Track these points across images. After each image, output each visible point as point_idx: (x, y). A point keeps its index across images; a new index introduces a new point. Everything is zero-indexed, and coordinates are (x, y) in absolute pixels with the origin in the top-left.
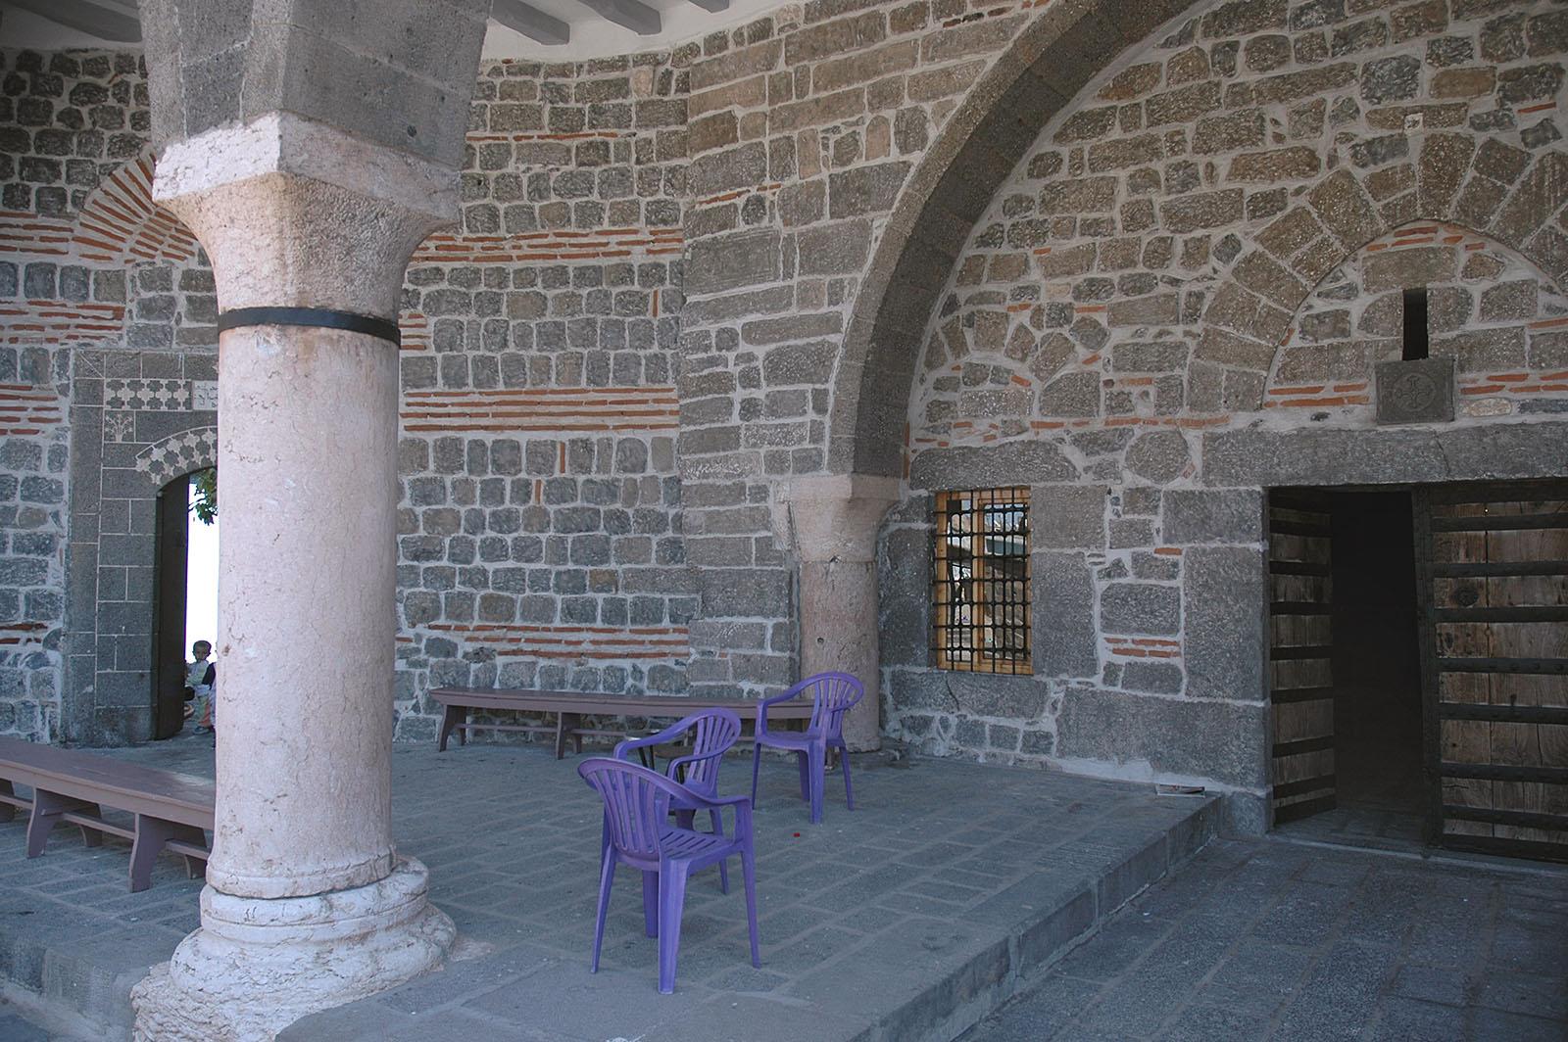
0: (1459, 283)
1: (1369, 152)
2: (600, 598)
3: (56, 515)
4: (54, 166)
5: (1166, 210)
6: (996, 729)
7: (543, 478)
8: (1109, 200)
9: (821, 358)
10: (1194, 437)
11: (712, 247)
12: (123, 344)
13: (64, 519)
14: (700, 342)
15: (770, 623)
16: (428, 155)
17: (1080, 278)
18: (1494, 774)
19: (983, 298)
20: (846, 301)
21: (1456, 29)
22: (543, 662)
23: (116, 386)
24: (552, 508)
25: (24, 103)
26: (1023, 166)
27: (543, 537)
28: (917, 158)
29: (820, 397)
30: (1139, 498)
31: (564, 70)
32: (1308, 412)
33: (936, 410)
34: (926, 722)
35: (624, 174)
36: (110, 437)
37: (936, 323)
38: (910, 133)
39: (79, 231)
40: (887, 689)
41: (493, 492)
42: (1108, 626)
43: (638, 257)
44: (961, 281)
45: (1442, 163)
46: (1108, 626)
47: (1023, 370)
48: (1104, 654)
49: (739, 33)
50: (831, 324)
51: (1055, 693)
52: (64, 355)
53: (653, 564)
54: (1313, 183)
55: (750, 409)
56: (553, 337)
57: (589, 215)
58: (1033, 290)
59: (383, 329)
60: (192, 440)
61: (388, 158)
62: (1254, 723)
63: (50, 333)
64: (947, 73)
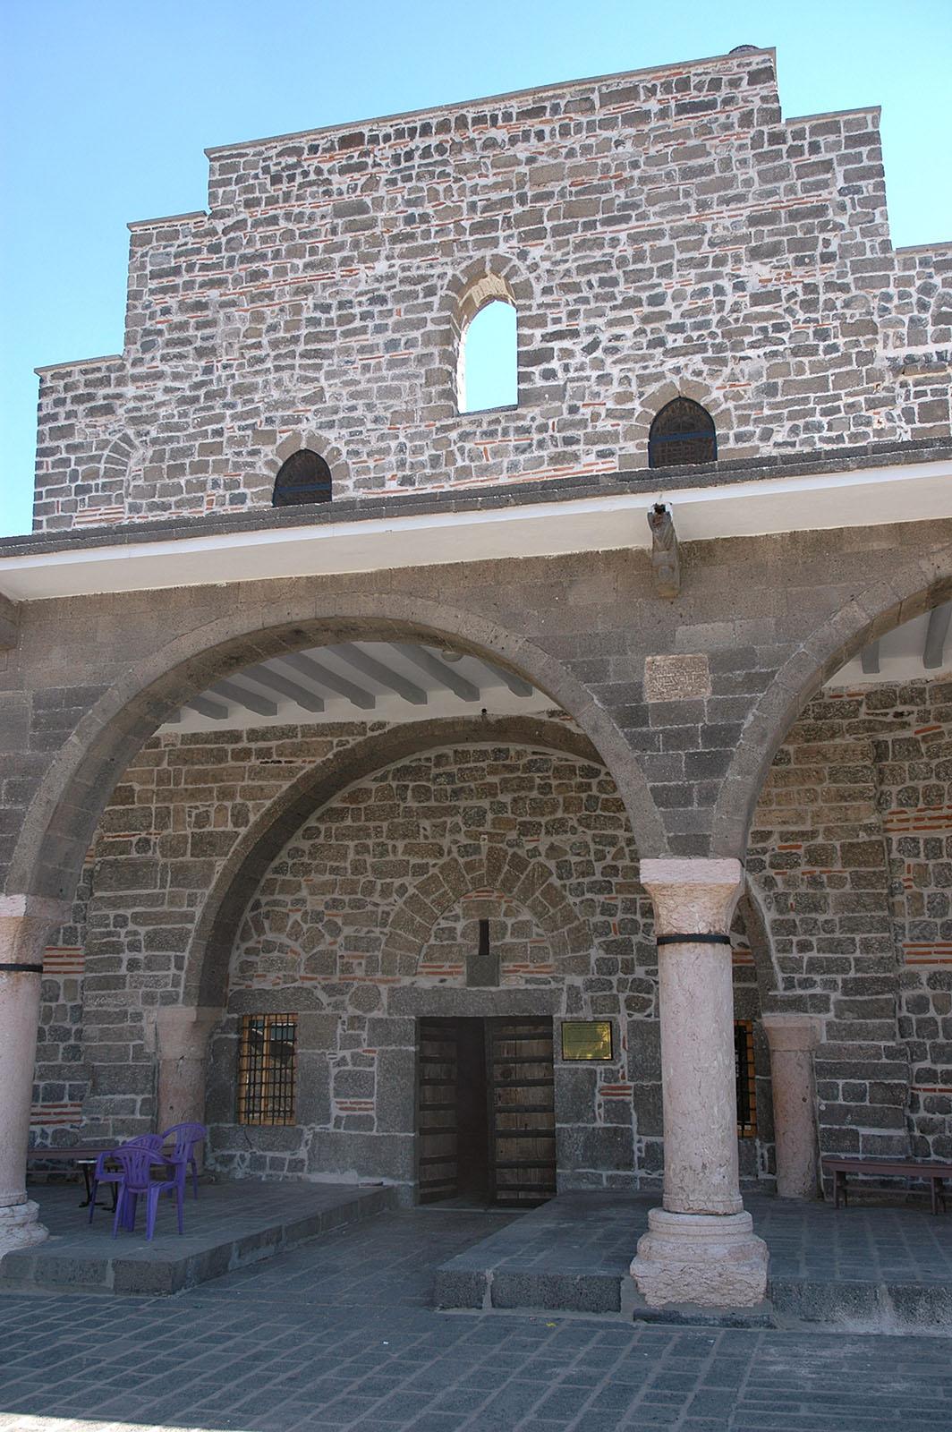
0: (503, 919)
1: (465, 850)
6: (273, 1159)
8: (345, 857)
9: (182, 937)
10: (383, 988)
15: (139, 1098)
17: (328, 897)
18: (517, 1165)
19: (276, 903)
20: (198, 905)
26: (300, 832)
28: (243, 830)
29: (179, 961)
30: (355, 1021)
34: (231, 1158)
37: (248, 915)
38: (240, 817)
42: (337, 1095)
44: (263, 892)
45: (495, 859)
47: (296, 946)
48: (335, 1111)
50: (188, 918)
51: (308, 1136)
53: (59, 1062)
54: (441, 862)
55: (133, 964)
59: (37, 969)
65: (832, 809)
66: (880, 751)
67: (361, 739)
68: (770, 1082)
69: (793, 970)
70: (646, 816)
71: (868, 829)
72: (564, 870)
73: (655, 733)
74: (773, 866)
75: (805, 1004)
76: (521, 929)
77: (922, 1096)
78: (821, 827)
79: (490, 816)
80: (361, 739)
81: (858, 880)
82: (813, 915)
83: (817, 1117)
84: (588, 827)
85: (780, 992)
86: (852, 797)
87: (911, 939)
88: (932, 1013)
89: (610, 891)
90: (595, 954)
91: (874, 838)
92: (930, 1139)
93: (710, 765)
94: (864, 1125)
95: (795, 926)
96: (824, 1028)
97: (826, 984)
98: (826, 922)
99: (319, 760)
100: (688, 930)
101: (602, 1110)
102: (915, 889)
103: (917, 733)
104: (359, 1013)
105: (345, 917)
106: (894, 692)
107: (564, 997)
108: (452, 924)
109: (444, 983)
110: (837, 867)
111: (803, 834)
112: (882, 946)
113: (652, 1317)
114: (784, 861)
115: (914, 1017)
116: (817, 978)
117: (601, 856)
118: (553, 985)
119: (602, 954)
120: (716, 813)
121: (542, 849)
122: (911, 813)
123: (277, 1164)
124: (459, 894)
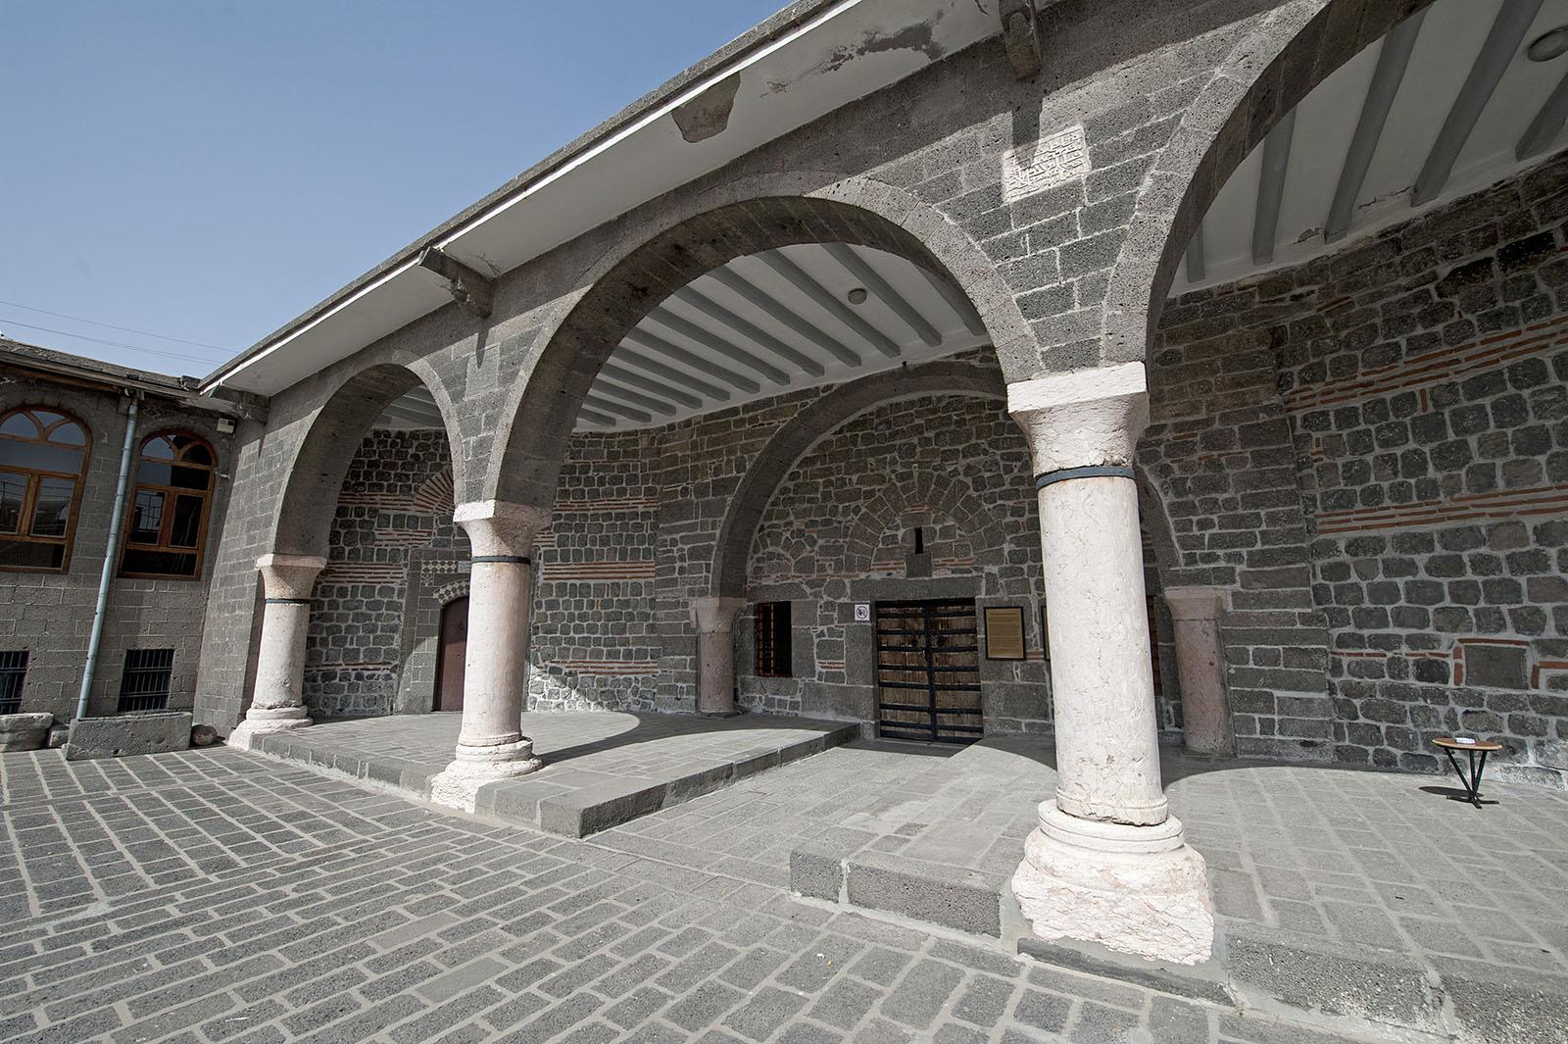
0: (932, 525)
1: (902, 477)
2: (622, 649)
3: (399, 616)
4: (407, 476)
5: (836, 494)
6: (780, 700)
7: (600, 599)
8: (816, 490)
10: (846, 581)
11: (667, 506)
12: (431, 546)
13: (402, 618)
14: (664, 543)
15: (688, 658)
16: (542, 506)
17: (807, 519)
18: (953, 711)
21: (926, 435)
22: (598, 676)
23: (427, 564)
24: (603, 611)
25: (397, 452)
27: (599, 624)
29: (708, 565)
30: (829, 606)
31: (613, 435)
32: (886, 572)
33: (757, 570)
34: (754, 698)
35: (636, 476)
36: (423, 584)
37: (756, 535)
38: (740, 468)
39: (416, 501)
40: (739, 685)
41: (579, 605)
42: (818, 658)
43: (640, 509)
44: (765, 520)
45: (925, 480)
46: (818, 658)
48: (818, 668)
49: (679, 424)
50: (712, 537)
52: (406, 551)
53: (644, 634)
54: (884, 487)
55: (682, 570)
56: (605, 542)
57: (622, 492)
58: (790, 524)
60: (456, 585)
61: (528, 509)
62: (871, 694)
63: (401, 542)
64: (752, 444)
65: (1226, 397)
66: (1276, 337)
67: (816, 399)
68: (1174, 648)
69: (1194, 547)
70: (1010, 330)
71: (1269, 410)
72: (979, 484)
73: (1019, 235)
74: (1167, 455)
75: (1209, 577)
76: (946, 532)
77: (1345, 661)
78: (1217, 415)
79: (918, 449)
80: (816, 399)
81: (1258, 458)
82: (1214, 495)
83: (1225, 681)
84: (997, 448)
85: (1181, 567)
86: (1251, 381)
87: (1325, 509)
88: (1354, 578)
89: (1018, 497)
90: (1007, 547)
91: (1275, 417)
92: (1357, 702)
93: (1100, 252)
94: (1278, 687)
95: (1195, 506)
96: (1230, 598)
97: (1229, 557)
98: (1226, 500)
99: (789, 419)
100: (1073, 461)
101: (1019, 671)
102: (1326, 460)
103: (1319, 310)
104: (831, 599)
105: (819, 531)
106: (1290, 277)
107: (984, 582)
108: (893, 532)
109: (891, 575)
110: (1237, 449)
111: (1198, 422)
112: (1291, 517)
113: (1041, 952)
114: (1180, 448)
115: (1331, 585)
116: (1220, 552)
117: (1009, 470)
118: (974, 573)
119: (1013, 546)
120: (1106, 310)
121: (961, 470)
122: (1318, 387)
123: (782, 703)
124: (897, 509)
